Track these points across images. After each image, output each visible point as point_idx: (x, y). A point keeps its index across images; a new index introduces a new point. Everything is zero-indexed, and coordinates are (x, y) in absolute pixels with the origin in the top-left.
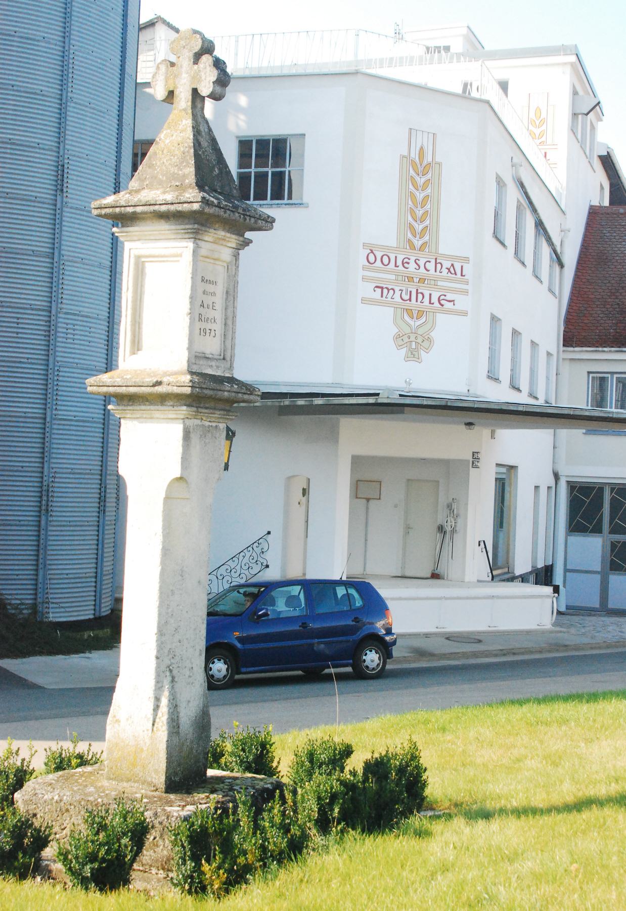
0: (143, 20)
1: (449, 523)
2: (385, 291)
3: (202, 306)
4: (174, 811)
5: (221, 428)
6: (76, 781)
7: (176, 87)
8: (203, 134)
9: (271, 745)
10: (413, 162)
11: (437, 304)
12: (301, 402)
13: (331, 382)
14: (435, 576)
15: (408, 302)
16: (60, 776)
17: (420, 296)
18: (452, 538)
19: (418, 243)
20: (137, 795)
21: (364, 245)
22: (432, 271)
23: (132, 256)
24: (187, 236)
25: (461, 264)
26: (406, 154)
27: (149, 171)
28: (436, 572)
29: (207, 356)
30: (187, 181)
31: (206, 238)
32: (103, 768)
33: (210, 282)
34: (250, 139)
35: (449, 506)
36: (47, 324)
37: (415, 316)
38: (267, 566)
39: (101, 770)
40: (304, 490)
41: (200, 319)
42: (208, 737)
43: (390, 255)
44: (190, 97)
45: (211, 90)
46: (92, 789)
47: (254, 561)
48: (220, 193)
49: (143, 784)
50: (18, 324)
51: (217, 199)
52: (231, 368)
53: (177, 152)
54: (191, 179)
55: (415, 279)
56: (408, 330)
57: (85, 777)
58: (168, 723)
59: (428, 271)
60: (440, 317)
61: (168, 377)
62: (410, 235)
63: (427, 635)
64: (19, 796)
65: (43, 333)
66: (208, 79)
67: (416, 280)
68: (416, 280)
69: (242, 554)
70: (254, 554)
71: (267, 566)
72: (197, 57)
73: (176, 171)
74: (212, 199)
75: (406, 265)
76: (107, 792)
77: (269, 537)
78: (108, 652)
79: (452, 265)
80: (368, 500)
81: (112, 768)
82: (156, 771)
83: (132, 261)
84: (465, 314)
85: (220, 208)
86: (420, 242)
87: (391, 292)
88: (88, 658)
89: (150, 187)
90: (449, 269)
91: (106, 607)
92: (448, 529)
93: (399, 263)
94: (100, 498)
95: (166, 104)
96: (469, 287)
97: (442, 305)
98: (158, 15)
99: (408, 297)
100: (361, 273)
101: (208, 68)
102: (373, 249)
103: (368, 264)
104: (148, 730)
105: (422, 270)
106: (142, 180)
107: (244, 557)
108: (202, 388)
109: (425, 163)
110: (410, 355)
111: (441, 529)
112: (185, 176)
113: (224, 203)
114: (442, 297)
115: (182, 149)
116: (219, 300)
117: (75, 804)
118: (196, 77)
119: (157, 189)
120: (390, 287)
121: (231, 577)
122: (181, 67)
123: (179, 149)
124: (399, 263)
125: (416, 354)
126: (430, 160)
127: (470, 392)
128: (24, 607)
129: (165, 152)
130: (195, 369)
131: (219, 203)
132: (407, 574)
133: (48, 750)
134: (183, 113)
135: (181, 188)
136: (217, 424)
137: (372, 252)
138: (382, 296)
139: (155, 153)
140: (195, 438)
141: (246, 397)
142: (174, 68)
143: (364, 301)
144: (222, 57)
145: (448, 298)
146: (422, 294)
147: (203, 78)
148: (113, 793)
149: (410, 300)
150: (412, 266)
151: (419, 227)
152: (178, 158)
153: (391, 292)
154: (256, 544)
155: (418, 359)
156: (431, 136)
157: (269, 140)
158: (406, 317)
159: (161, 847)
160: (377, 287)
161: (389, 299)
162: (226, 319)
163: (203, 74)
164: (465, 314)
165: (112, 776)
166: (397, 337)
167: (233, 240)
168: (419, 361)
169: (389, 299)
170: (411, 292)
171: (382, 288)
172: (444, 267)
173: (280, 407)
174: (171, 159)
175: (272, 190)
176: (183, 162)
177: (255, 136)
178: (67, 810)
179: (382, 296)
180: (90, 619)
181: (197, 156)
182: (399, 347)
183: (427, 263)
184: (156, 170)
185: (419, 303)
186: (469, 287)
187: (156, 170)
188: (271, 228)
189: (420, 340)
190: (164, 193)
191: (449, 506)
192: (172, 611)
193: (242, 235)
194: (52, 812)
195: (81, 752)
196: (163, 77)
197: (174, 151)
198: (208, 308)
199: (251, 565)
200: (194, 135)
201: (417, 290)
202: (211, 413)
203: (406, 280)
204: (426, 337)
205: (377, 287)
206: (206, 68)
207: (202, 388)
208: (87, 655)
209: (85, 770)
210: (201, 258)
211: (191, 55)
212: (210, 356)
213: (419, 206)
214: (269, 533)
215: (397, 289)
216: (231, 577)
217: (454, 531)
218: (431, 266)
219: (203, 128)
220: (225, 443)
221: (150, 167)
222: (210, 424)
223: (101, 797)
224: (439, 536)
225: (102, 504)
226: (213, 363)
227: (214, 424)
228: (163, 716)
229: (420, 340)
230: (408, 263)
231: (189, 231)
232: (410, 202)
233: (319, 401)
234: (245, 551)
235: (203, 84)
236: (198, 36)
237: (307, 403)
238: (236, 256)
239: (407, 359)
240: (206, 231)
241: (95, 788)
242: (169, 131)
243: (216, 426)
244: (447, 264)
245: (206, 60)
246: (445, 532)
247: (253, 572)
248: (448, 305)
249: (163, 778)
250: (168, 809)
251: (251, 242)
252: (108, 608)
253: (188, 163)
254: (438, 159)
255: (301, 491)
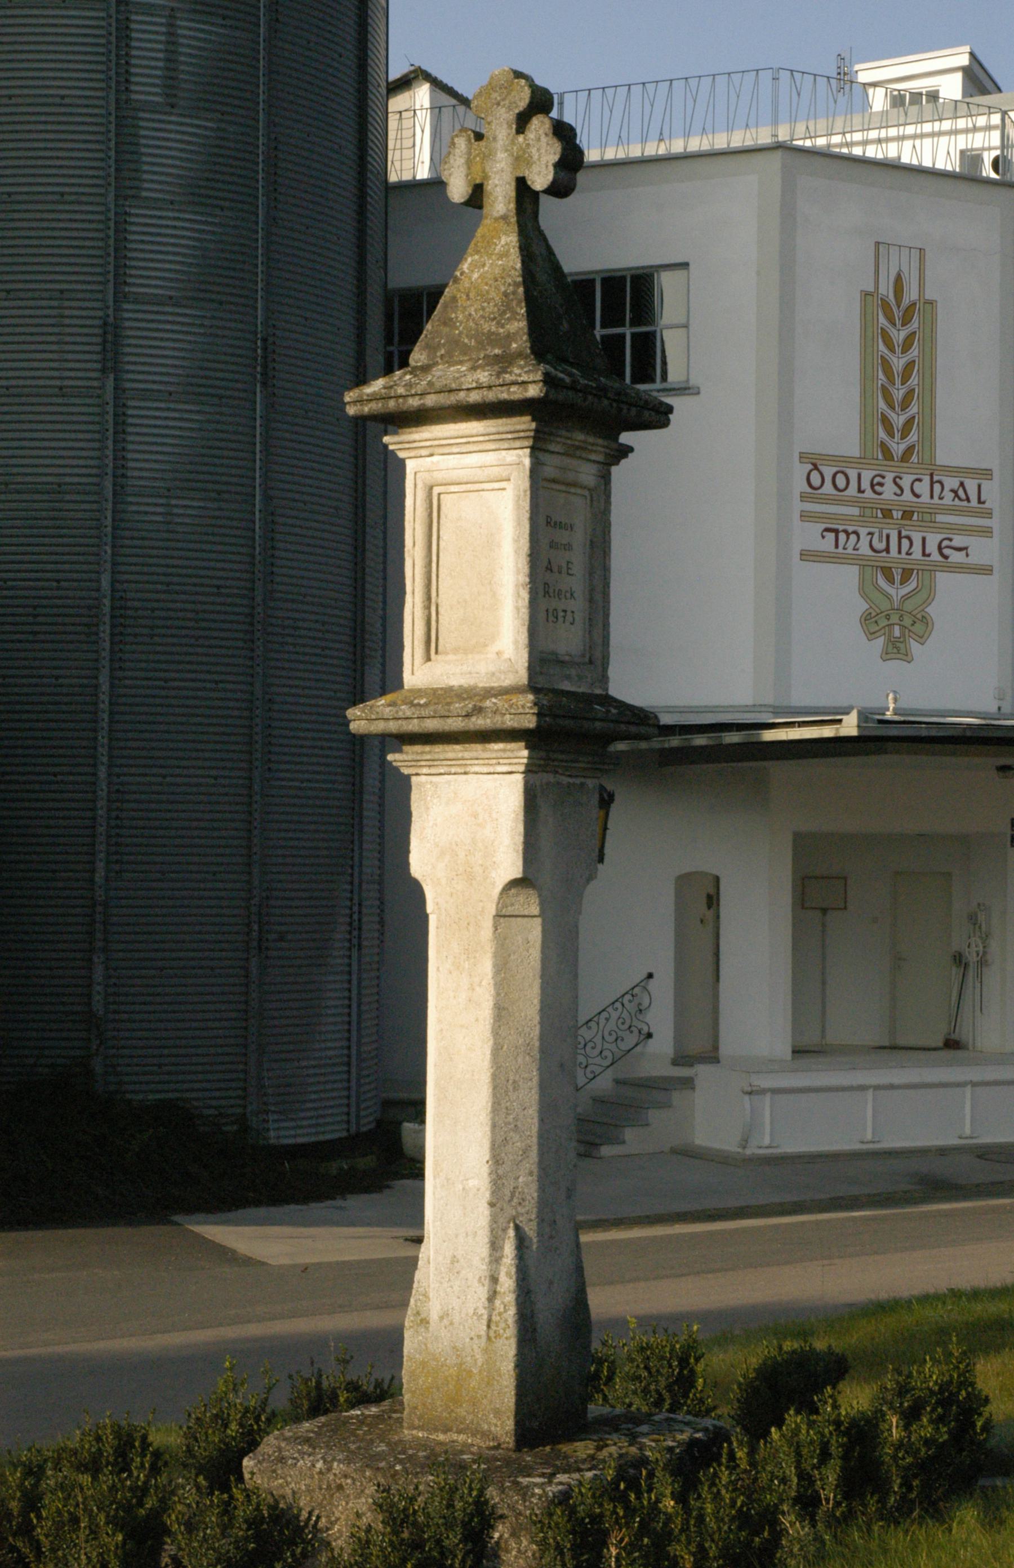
0: (395, 73)
1: (974, 949)
2: (842, 537)
3: (549, 569)
4: (536, 1485)
5: (591, 786)
6: (353, 1433)
7: (486, 177)
8: (539, 259)
9: (697, 1360)
10: (885, 305)
11: (936, 556)
12: (700, 740)
13: (750, 702)
14: (952, 1044)
15: (884, 554)
16: (324, 1425)
17: (905, 543)
18: (980, 976)
19: (898, 448)
20: (465, 1457)
21: (803, 457)
22: (925, 498)
23: (420, 485)
24: (518, 444)
25: (977, 481)
26: (871, 288)
27: (445, 330)
28: (953, 1037)
29: (562, 658)
30: (514, 345)
31: (552, 447)
32: (398, 1407)
33: (559, 525)
34: (591, 277)
35: (973, 918)
36: (248, 620)
37: (897, 578)
38: (649, 1035)
39: (395, 1412)
40: (709, 897)
41: (546, 593)
42: (587, 1346)
43: (849, 471)
44: (513, 194)
45: (550, 177)
46: (383, 1447)
47: (626, 1026)
48: (572, 364)
49: (474, 1435)
50: (196, 621)
51: (570, 374)
52: (604, 679)
53: (493, 294)
54: (521, 343)
55: (894, 513)
56: (885, 605)
57: (368, 1425)
58: (517, 1322)
59: (917, 496)
60: (943, 579)
61: (494, 700)
62: (882, 434)
63: (943, 1152)
64: (252, 1463)
65: (241, 635)
66: (544, 160)
67: (897, 515)
68: (897, 515)
69: (605, 1015)
70: (625, 1014)
71: (649, 1035)
72: (522, 122)
73: (493, 329)
74: (562, 375)
75: (877, 488)
76: (410, 1452)
77: (652, 985)
78: (374, 1196)
79: (962, 484)
80: (824, 911)
81: (416, 1408)
82: (497, 1413)
83: (421, 495)
84: (986, 570)
85: (577, 391)
86: (903, 447)
87: (853, 538)
88: (341, 1208)
89: (449, 360)
90: (955, 492)
91: (367, 1116)
92: (973, 959)
93: (866, 484)
94: (350, 924)
95: (470, 209)
96: (994, 523)
97: (946, 557)
98: (417, 64)
99: (883, 546)
100: (798, 506)
101: (544, 139)
102: (819, 462)
103: (809, 490)
104: (479, 1337)
105: (908, 495)
106: (431, 348)
107: (607, 1019)
108: (555, 716)
109: (905, 302)
110: (890, 650)
111: (958, 959)
112: (509, 337)
113: (583, 381)
114: (945, 543)
115: (503, 289)
116: (578, 558)
117: (354, 1475)
118: (520, 159)
119: (461, 363)
120: (850, 529)
121: (586, 1056)
122: (495, 139)
123: (497, 288)
124: (866, 484)
125: (902, 646)
126: (914, 296)
127: (1003, 710)
128: (224, 1121)
129: (471, 295)
130: (541, 682)
131: (574, 382)
132: (902, 1042)
133: (295, 1376)
134: (502, 222)
135: (503, 362)
136: (583, 780)
137: (816, 467)
138: (837, 546)
139: (454, 299)
140: (545, 810)
141: (633, 729)
142: (483, 143)
143: (806, 555)
144: (568, 118)
145: (954, 543)
146: (909, 538)
147: (536, 157)
148: (421, 1454)
149: (887, 550)
150: (889, 490)
151: (898, 420)
152: (496, 305)
153: (853, 538)
154: (628, 997)
155: (906, 657)
156: (915, 253)
157: (623, 278)
158: (882, 582)
159: (514, 1553)
160: (827, 530)
161: (850, 551)
162: (592, 590)
163: (534, 151)
164: (986, 570)
165: (416, 1422)
166: (867, 618)
167: (598, 445)
168: (909, 658)
169: (850, 551)
170: (888, 537)
171: (836, 532)
172: (947, 489)
173: (662, 751)
174: (483, 309)
175: (633, 366)
176: (504, 312)
177: (597, 272)
178: (340, 1487)
179: (837, 546)
180: (340, 1139)
181: (530, 300)
182: (871, 635)
183: (917, 483)
184: (457, 328)
185: (903, 555)
186: (994, 523)
187: (457, 328)
188: (665, 424)
189: (907, 621)
190: (474, 368)
191: (973, 918)
192: (516, 1119)
193: (616, 439)
194: (313, 1491)
195: (355, 1379)
196: (463, 161)
197: (488, 292)
198: (560, 572)
199: (620, 1033)
200: (523, 262)
201: (900, 533)
202: (572, 761)
203: (880, 515)
204: (919, 616)
205: (827, 530)
206: (539, 140)
207: (555, 716)
208: (339, 1202)
209: (367, 1413)
210: (546, 484)
211: (511, 116)
212: (567, 658)
213: (898, 381)
214: (650, 976)
215: (863, 532)
216: (586, 1056)
217: (983, 962)
218: (923, 488)
219: (537, 249)
220: (596, 812)
221: (445, 324)
222: (571, 780)
223: (401, 1462)
224: (955, 972)
225: (355, 933)
226: (573, 672)
227: (578, 781)
228: (505, 1311)
229: (907, 621)
230: (881, 485)
231: (522, 434)
232: (881, 375)
233: (733, 738)
234: (610, 1009)
235: (535, 169)
236: (523, 82)
237: (711, 743)
238: (606, 478)
239: (886, 655)
240: (551, 434)
241: (388, 1444)
242: (476, 257)
243: (582, 784)
244: (951, 483)
245: (539, 125)
246: (966, 965)
247: (624, 1046)
248: (956, 557)
249: (510, 1424)
250: (524, 1481)
251: (631, 449)
252: (371, 1119)
253: (515, 313)
254: (929, 295)
255: (704, 901)
